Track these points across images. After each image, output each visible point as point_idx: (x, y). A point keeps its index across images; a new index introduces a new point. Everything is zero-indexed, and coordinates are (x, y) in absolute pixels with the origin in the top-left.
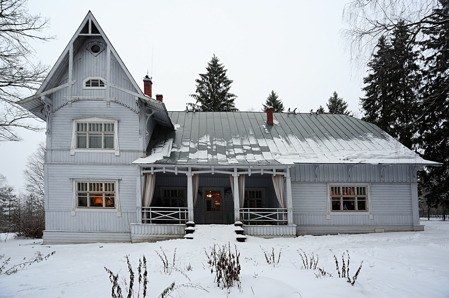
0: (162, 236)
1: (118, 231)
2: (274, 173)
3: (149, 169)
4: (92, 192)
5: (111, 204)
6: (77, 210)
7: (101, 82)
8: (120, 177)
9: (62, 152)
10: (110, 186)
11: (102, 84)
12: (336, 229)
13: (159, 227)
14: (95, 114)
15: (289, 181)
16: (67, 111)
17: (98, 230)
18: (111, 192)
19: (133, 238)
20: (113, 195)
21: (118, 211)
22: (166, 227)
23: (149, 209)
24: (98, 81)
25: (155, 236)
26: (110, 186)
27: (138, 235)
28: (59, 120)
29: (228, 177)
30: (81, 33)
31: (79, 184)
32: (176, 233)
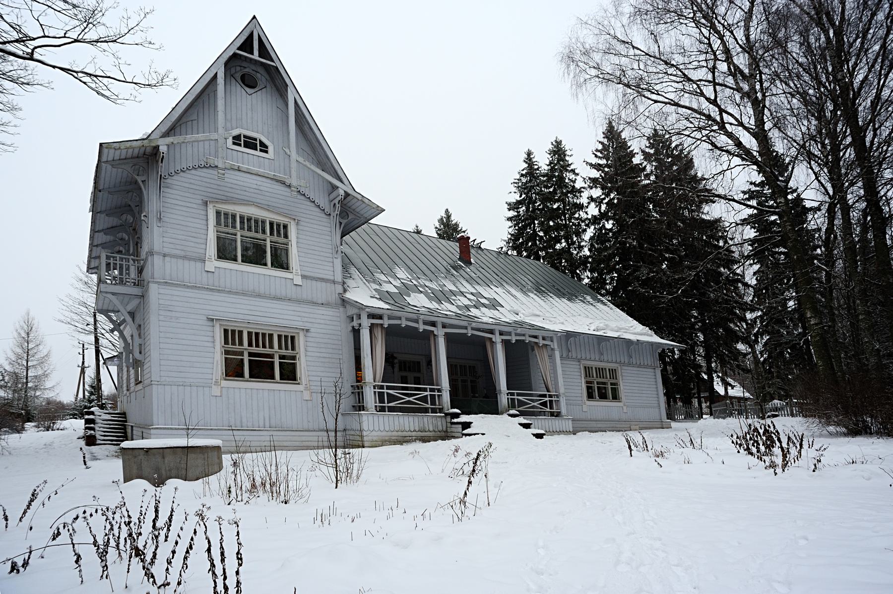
0: (410, 434)
1: (306, 427)
2: (541, 342)
3: (380, 317)
4: (254, 349)
5: (289, 374)
6: (225, 383)
7: (262, 144)
8: (308, 326)
9: (186, 262)
10: (289, 341)
11: (264, 148)
12: (593, 425)
13: (406, 418)
14: (254, 200)
15: (557, 354)
16: (192, 181)
17: (267, 425)
18: (289, 352)
19: (365, 439)
20: (294, 358)
21: (306, 389)
22: (416, 419)
23: (382, 387)
24: (256, 140)
25: (400, 434)
26: (289, 341)
27: (374, 433)
28: (178, 197)
29: (427, 337)
30: (239, 49)
31: (226, 331)
32: (431, 429)
